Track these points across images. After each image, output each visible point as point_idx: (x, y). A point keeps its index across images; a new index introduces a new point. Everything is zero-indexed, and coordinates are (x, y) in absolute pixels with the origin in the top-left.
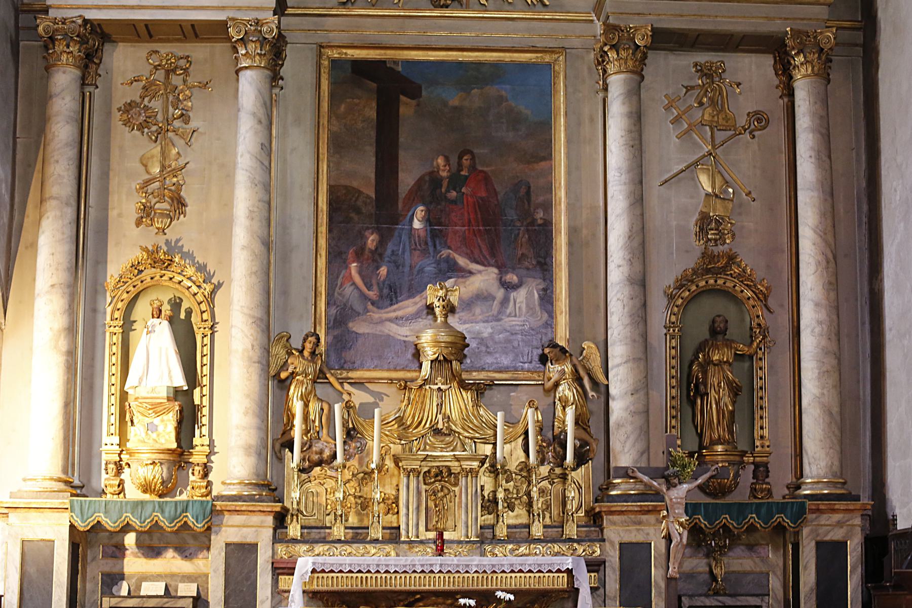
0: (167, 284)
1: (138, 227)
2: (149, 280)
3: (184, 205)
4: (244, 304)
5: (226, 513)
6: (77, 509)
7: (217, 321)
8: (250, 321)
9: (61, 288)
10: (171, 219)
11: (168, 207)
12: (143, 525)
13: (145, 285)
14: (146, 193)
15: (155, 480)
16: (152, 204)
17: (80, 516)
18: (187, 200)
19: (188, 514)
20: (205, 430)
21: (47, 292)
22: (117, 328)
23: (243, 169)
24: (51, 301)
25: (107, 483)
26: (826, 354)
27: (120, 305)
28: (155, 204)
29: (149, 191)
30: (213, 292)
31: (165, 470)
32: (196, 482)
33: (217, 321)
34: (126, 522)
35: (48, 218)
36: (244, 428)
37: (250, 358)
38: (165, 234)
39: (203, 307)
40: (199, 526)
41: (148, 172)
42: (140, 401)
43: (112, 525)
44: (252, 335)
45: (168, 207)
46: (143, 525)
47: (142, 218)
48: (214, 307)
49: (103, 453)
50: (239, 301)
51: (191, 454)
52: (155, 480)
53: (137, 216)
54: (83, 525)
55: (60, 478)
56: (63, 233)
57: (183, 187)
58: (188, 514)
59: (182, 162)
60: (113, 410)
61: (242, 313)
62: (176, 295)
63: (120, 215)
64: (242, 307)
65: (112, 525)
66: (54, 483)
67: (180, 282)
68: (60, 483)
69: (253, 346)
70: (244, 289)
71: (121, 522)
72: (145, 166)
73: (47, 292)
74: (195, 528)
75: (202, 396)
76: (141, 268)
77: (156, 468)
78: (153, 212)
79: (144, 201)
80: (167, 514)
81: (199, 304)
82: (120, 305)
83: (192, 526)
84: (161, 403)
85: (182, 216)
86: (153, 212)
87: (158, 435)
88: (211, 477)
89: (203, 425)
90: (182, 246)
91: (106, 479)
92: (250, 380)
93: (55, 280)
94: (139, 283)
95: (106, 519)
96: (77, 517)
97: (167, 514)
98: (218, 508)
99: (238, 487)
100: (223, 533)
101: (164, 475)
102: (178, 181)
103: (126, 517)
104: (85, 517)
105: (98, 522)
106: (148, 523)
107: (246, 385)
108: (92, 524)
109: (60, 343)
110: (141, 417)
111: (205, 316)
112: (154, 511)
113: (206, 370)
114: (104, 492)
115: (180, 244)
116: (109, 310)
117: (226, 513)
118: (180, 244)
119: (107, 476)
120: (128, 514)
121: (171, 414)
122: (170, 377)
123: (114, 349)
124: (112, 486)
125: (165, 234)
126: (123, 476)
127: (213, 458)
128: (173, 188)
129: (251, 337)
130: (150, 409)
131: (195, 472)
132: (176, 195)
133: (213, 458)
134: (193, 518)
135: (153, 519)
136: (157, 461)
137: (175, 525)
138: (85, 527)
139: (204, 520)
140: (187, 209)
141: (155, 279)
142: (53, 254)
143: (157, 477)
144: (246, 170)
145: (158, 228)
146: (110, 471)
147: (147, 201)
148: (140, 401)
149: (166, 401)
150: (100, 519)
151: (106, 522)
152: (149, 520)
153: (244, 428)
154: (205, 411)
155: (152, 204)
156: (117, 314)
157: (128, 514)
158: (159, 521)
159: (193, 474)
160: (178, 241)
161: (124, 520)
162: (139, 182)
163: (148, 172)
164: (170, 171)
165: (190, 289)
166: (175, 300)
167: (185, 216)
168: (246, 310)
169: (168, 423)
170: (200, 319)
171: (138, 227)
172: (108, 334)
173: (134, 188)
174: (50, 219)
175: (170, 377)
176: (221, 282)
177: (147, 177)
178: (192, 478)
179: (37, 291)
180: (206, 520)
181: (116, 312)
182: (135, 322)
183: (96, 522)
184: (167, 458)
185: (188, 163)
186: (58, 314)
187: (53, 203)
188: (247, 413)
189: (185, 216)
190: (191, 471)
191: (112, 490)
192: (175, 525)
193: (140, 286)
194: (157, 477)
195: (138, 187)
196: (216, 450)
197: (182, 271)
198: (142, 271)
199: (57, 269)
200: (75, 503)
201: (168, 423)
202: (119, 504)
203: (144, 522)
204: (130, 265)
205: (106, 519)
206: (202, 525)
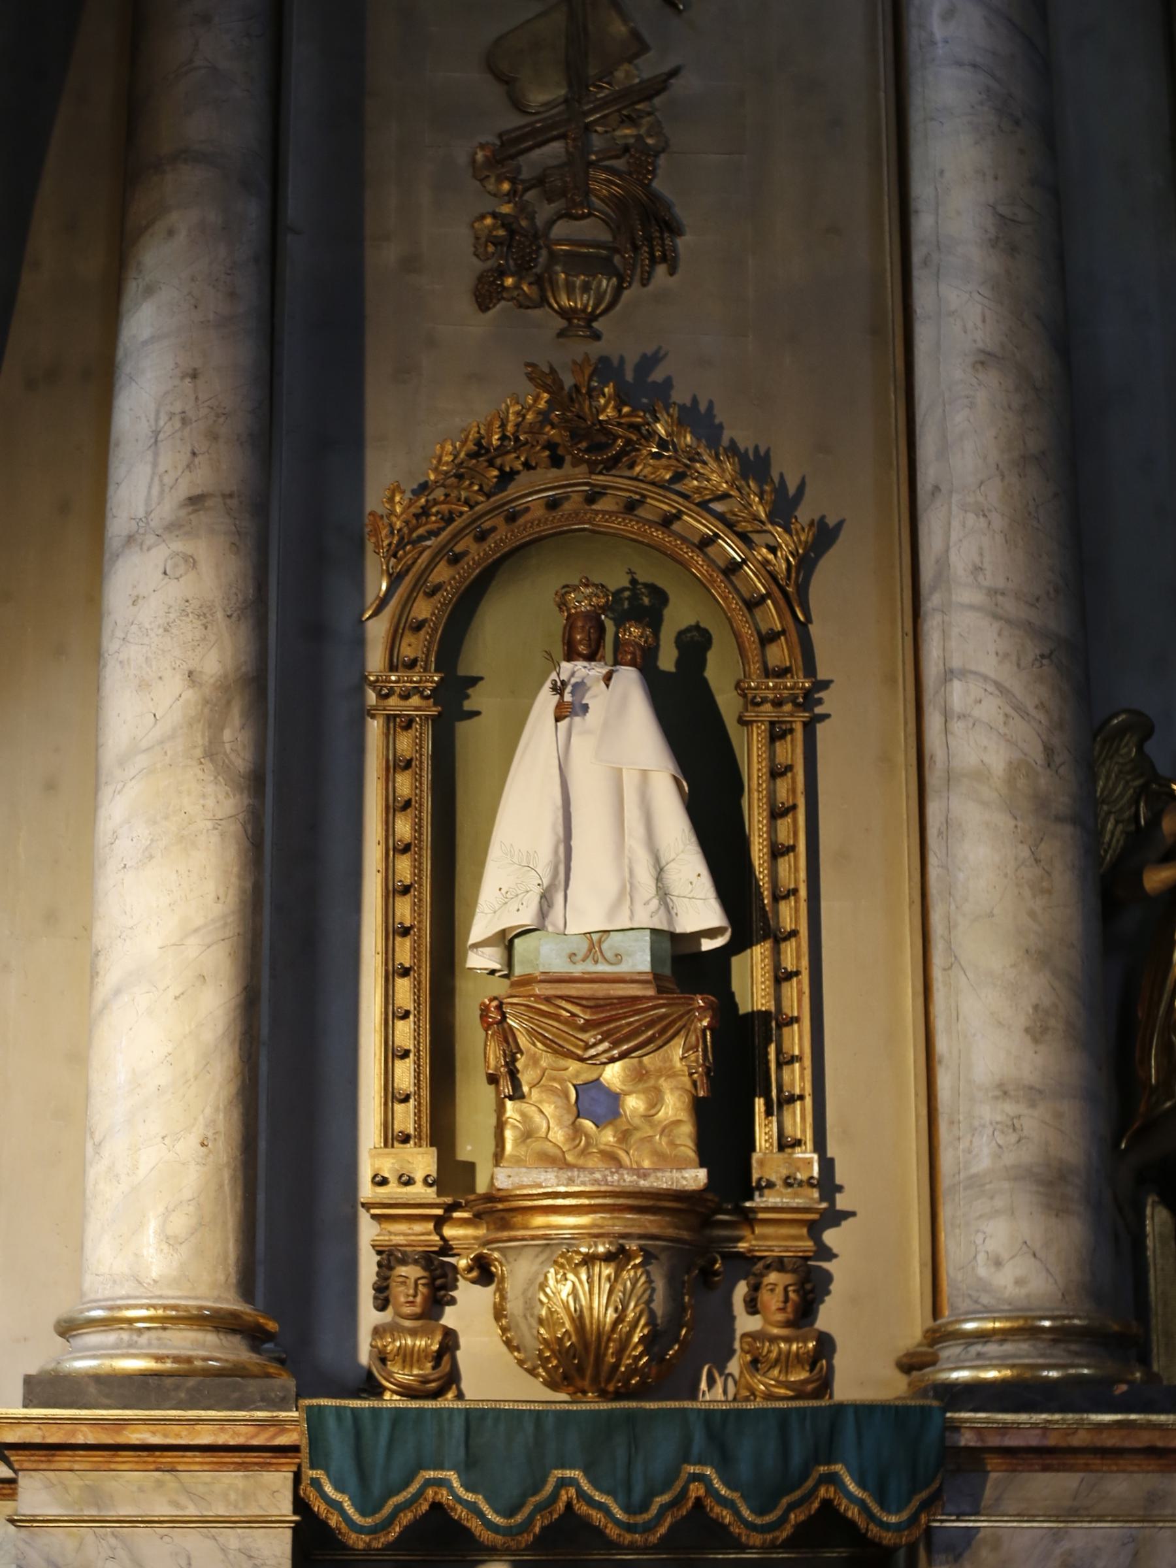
0: (616, 525)
1: (484, 307)
2: (538, 512)
3: (672, 228)
4: (1001, 583)
5: (992, 1462)
6: (339, 1447)
7: (822, 675)
8: (1032, 650)
9: (229, 511)
10: (621, 279)
11: (605, 236)
12: (641, 1519)
13: (521, 533)
14: (513, 181)
15: (623, 1328)
16: (540, 221)
17: (352, 1481)
18: (678, 211)
19: (838, 1468)
20: (798, 1120)
21: (173, 527)
22: (415, 700)
23: (959, 64)
24: (191, 562)
25: (393, 1345)
26: (1057, 1215)
27: (423, 609)
28: (551, 223)
29: (524, 175)
30: (806, 564)
31: (660, 1284)
32: (774, 1339)
33: (822, 675)
34: (561, 1505)
35: (171, 233)
36: (1033, 1095)
37: (1041, 804)
38: (597, 336)
39: (771, 616)
40: (893, 1519)
41: (519, 106)
42: (538, 990)
43: (498, 1520)
44: (1041, 706)
45: (605, 236)
46: (641, 1519)
47: (502, 273)
48: (809, 619)
49: (364, 1217)
50: (978, 569)
51: (748, 1219)
52: (623, 1328)
53: (479, 265)
54: (368, 1521)
55: (235, 1315)
56: (232, 295)
57: (662, 160)
58: (838, 1468)
59: (647, 68)
60: (404, 1033)
61: (996, 617)
62: (642, 578)
63: (411, 263)
64: (993, 592)
65: (498, 1520)
66: (211, 1338)
67: (667, 521)
68: (236, 1340)
69: (1049, 751)
70: (998, 522)
71: (539, 1508)
72: (506, 81)
73: (173, 527)
74: (874, 1530)
75: (781, 977)
76: (512, 461)
77: (627, 1275)
78: (544, 252)
79: (506, 209)
80: (744, 1470)
81: (753, 604)
82: (423, 609)
83: (861, 1522)
84: (635, 999)
85: (661, 270)
86: (544, 252)
87: (624, 1137)
88: (827, 1318)
89: (792, 1099)
90: (668, 383)
91: (377, 1332)
92: (1049, 892)
93: (202, 478)
94: (499, 521)
95: (470, 1497)
96: (339, 1488)
97: (744, 1470)
98: (967, 1439)
99: (1024, 1346)
100: (984, 1553)
101: (658, 1306)
102: (639, 138)
103: (563, 1483)
104: (377, 1488)
105: (436, 1506)
106: (664, 1509)
107: (1032, 914)
108: (407, 1518)
109: (227, 735)
110: (546, 1060)
111: (778, 654)
112: (686, 1460)
113: (793, 872)
114: (372, 1387)
115: (658, 376)
116: (377, 630)
117: (992, 1462)
118: (658, 376)
119: (386, 1316)
120: (569, 1473)
121: (676, 1050)
122: (663, 894)
123: (404, 784)
124: (408, 1357)
125: (597, 336)
126: (450, 1318)
127: (830, 1237)
128: (620, 164)
129: (1041, 716)
130: (588, 1026)
131: (765, 1296)
132: (639, 192)
133: (830, 1237)
134: (862, 1484)
135: (684, 1491)
136: (633, 1246)
137: (783, 1519)
138: (374, 1530)
139: (913, 1492)
140: (680, 242)
141: (567, 506)
142: (194, 375)
143: (631, 1315)
144: (974, 66)
145: (564, 313)
146: (400, 1294)
147: (522, 208)
148: (538, 990)
149: (651, 992)
150: (444, 1496)
151: (473, 1508)
152: (665, 1498)
153: (1033, 1095)
154: (797, 1040)
155: (540, 221)
156: (410, 648)
157: (569, 1473)
158: (708, 1502)
159: (752, 1306)
160: (648, 362)
161: (555, 1496)
162: (484, 139)
163: (519, 106)
164: (605, 103)
165: (711, 550)
166: (635, 597)
167: (672, 272)
168: (1010, 606)
169: (665, 1085)
170: (755, 668)
171: (484, 307)
172: (374, 727)
173: (462, 159)
174: (182, 237)
175: (663, 894)
176: (831, 522)
177: (515, 121)
178: (746, 1323)
179: (118, 524)
180: (924, 1495)
181: (409, 638)
182: (474, 681)
183: (425, 1507)
184: (670, 1232)
185: (674, 73)
186: (220, 615)
187: (191, 176)
188: (1045, 1030)
189: (672, 272)
190: (741, 1289)
191: (403, 1375)
192: (783, 1519)
193: (504, 536)
194: (631, 1315)
195: (480, 156)
196: (842, 1202)
197: (678, 477)
198: (513, 473)
199: (213, 436)
200: (331, 1423)
201: (665, 1085)
202: (529, 1428)
203: (644, 1507)
204: (471, 446)
205: (470, 1497)
206: (904, 1516)
